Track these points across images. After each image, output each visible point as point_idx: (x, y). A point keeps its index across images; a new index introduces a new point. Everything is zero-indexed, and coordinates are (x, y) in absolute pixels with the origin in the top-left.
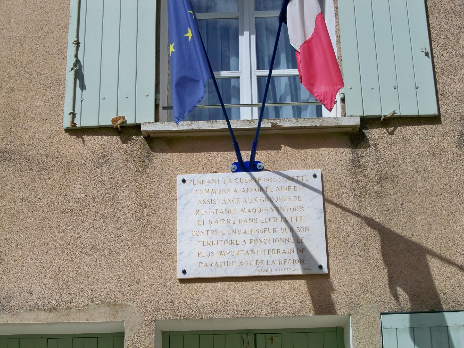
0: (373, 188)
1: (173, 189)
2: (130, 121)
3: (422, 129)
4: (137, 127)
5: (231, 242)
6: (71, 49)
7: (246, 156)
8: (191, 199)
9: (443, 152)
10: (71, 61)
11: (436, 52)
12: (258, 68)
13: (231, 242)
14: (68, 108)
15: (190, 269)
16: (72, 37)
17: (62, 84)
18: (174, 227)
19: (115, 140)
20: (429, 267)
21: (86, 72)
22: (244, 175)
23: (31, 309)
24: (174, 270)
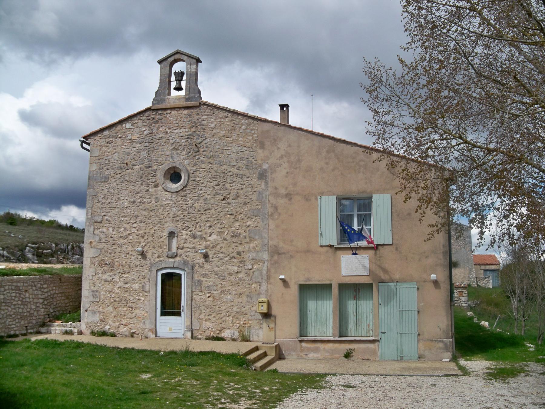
0: (378, 258)
1: (340, 259)
2: (332, 245)
3: (389, 246)
4: (333, 246)
5: (351, 269)
6: (319, 228)
7: (354, 252)
8: (267, 163)
9: (392, 251)
10: (320, 232)
11: (393, 230)
12: (358, 226)
13: (351, 269)
14: (320, 242)
15: (409, 214)
16: (319, 226)
17: (318, 236)
18: (341, 266)
19: (329, 248)
20: (17, 217)
21: (323, 234)
22: (354, 256)
23: (315, 281)
24: (341, 274)
